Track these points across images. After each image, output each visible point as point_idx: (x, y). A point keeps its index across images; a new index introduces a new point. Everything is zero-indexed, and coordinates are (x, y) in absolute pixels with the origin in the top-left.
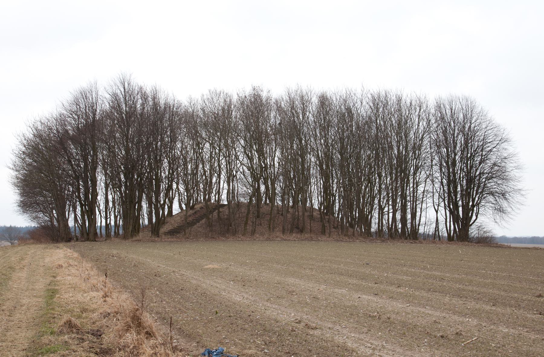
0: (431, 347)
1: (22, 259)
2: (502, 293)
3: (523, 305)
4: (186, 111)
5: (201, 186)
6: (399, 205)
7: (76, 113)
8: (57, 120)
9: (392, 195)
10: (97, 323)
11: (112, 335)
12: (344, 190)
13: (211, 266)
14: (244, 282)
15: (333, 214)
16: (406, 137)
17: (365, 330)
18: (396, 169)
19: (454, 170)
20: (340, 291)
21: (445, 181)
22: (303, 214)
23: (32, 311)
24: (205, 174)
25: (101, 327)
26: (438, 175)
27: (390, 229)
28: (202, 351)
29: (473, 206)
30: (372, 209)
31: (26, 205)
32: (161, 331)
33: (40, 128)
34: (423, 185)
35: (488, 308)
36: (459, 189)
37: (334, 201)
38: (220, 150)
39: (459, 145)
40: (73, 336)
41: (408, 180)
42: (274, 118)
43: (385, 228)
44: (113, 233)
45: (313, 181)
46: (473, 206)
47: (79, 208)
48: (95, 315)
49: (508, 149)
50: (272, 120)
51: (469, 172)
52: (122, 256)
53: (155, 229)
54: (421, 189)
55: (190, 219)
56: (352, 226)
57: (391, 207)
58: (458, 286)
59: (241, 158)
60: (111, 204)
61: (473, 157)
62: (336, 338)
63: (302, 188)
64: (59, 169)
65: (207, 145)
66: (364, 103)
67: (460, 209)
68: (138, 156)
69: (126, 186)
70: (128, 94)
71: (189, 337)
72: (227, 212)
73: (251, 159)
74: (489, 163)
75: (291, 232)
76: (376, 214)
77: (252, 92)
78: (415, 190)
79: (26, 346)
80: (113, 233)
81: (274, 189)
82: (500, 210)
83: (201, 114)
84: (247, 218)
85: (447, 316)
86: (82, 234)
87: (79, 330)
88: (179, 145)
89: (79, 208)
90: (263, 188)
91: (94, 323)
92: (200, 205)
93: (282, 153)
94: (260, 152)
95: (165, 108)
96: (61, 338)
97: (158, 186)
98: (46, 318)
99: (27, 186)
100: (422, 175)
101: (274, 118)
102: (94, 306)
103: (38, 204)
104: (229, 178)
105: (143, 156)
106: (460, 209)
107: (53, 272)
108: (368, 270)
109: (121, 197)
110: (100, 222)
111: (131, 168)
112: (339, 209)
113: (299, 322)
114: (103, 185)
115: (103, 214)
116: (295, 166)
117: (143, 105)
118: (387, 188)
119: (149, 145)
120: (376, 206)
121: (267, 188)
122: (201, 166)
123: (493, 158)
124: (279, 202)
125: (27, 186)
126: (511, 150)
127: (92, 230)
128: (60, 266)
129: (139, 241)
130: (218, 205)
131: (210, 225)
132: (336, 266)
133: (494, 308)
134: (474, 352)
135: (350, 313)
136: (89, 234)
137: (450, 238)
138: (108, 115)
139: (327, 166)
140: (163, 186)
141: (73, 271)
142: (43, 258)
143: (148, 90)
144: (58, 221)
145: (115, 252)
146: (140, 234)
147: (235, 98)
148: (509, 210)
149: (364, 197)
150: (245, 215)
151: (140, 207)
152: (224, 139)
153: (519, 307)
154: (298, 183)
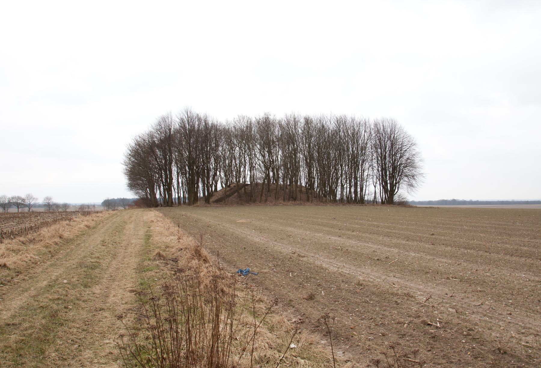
0: (371, 265)
1: (131, 217)
2: (412, 234)
3: (423, 240)
4: (224, 129)
5: (234, 173)
6: (353, 183)
7: (159, 130)
8: (148, 135)
9: (349, 178)
10: (175, 254)
11: (184, 261)
12: (321, 175)
13: (241, 221)
14: (261, 230)
15: (314, 189)
16: (357, 143)
17: (333, 257)
18: (351, 162)
19: (385, 162)
20: (318, 235)
21: (380, 169)
22: (296, 190)
23: (138, 247)
24: (236, 166)
25: (177, 257)
26: (375, 165)
27: (347, 198)
28: (237, 270)
29: (396, 183)
30: (337, 186)
31: (133, 185)
32: (212, 258)
33: (139, 140)
34: (367, 171)
35: (404, 242)
36: (388, 173)
37: (314, 181)
38: (245, 151)
39: (388, 147)
40: (162, 261)
41: (358, 168)
42: (277, 132)
43: (345, 198)
44: (182, 202)
45: (301, 169)
46: (396, 183)
47: (162, 188)
48: (173, 250)
49: (416, 149)
50: (277, 133)
51: (393, 163)
52: (188, 215)
53: (207, 199)
54: (366, 173)
55: (228, 193)
56: (325, 196)
57: (348, 184)
58: (387, 230)
59: (258, 156)
60: (181, 185)
61: (396, 154)
62: (316, 262)
63: (295, 174)
64: (150, 164)
65: (237, 148)
66: (332, 122)
67: (389, 185)
68: (196, 156)
69: (189, 173)
70: (190, 119)
71: (229, 262)
72: (250, 188)
73: (264, 156)
74: (405, 158)
75: (289, 200)
76: (339, 189)
77: (264, 116)
78: (362, 175)
79: (135, 267)
80: (182, 202)
81: (278, 174)
82: (411, 185)
83: (233, 129)
84: (262, 193)
85: (381, 247)
86: (164, 202)
87: (164, 258)
88: (220, 148)
89: (162, 188)
90: (271, 174)
91: (173, 254)
92: (234, 185)
93: (283, 153)
94: (270, 152)
95: (212, 126)
96: (154, 263)
97: (208, 173)
98: (145, 251)
99: (132, 174)
100: (366, 165)
101: (277, 132)
102: (173, 245)
103: (138, 185)
104: (251, 168)
105: (199, 155)
106: (389, 185)
107: (148, 225)
108: (335, 222)
109: (187, 180)
110: (175, 195)
111: (192, 162)
112: (317, 186)
113: (294, 253)
114: (176, 173)
115: (176, 191)
116: (291, 160)
117: (199, 125)
118: (346, 173)
119: (203, 149)
120: (339, 184)
121: (274, 174)
122: (234, 161)
123: (407, 155)
124: (281, 182)
125: (132, 174)
126: (417, 150)
127: (170, 200)
128: (152, 221)
129: (198, 206)
130: (245, 185)
131: (240, 197)
132: (316, 220)
133: (407, 242)
134: (396, 268)
135: (324, 247)
136: (168, 203)
137: (383, 203)
138: (177, 131)
139: (310, 160)
140: (211, 173)
141: (160, 224)
142: (143, 217)
143: (202, 116)
144: (150, 195)
145: (184, 213)
146: (198, 202)
147: (253, 120)
148: (416, 185)
149: (332, 179)
150: (261, 190)
151: (198, 186)
152: (248, 145)
153: (421, 241)
154: (293, 170)
